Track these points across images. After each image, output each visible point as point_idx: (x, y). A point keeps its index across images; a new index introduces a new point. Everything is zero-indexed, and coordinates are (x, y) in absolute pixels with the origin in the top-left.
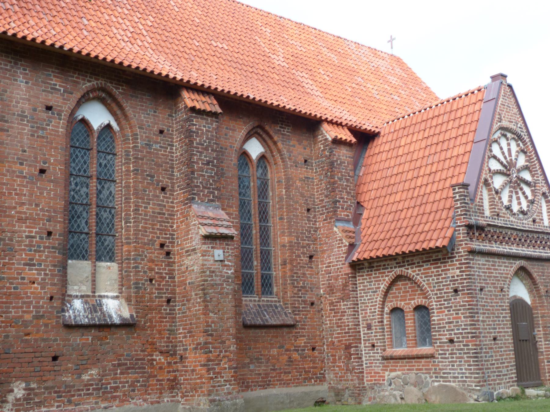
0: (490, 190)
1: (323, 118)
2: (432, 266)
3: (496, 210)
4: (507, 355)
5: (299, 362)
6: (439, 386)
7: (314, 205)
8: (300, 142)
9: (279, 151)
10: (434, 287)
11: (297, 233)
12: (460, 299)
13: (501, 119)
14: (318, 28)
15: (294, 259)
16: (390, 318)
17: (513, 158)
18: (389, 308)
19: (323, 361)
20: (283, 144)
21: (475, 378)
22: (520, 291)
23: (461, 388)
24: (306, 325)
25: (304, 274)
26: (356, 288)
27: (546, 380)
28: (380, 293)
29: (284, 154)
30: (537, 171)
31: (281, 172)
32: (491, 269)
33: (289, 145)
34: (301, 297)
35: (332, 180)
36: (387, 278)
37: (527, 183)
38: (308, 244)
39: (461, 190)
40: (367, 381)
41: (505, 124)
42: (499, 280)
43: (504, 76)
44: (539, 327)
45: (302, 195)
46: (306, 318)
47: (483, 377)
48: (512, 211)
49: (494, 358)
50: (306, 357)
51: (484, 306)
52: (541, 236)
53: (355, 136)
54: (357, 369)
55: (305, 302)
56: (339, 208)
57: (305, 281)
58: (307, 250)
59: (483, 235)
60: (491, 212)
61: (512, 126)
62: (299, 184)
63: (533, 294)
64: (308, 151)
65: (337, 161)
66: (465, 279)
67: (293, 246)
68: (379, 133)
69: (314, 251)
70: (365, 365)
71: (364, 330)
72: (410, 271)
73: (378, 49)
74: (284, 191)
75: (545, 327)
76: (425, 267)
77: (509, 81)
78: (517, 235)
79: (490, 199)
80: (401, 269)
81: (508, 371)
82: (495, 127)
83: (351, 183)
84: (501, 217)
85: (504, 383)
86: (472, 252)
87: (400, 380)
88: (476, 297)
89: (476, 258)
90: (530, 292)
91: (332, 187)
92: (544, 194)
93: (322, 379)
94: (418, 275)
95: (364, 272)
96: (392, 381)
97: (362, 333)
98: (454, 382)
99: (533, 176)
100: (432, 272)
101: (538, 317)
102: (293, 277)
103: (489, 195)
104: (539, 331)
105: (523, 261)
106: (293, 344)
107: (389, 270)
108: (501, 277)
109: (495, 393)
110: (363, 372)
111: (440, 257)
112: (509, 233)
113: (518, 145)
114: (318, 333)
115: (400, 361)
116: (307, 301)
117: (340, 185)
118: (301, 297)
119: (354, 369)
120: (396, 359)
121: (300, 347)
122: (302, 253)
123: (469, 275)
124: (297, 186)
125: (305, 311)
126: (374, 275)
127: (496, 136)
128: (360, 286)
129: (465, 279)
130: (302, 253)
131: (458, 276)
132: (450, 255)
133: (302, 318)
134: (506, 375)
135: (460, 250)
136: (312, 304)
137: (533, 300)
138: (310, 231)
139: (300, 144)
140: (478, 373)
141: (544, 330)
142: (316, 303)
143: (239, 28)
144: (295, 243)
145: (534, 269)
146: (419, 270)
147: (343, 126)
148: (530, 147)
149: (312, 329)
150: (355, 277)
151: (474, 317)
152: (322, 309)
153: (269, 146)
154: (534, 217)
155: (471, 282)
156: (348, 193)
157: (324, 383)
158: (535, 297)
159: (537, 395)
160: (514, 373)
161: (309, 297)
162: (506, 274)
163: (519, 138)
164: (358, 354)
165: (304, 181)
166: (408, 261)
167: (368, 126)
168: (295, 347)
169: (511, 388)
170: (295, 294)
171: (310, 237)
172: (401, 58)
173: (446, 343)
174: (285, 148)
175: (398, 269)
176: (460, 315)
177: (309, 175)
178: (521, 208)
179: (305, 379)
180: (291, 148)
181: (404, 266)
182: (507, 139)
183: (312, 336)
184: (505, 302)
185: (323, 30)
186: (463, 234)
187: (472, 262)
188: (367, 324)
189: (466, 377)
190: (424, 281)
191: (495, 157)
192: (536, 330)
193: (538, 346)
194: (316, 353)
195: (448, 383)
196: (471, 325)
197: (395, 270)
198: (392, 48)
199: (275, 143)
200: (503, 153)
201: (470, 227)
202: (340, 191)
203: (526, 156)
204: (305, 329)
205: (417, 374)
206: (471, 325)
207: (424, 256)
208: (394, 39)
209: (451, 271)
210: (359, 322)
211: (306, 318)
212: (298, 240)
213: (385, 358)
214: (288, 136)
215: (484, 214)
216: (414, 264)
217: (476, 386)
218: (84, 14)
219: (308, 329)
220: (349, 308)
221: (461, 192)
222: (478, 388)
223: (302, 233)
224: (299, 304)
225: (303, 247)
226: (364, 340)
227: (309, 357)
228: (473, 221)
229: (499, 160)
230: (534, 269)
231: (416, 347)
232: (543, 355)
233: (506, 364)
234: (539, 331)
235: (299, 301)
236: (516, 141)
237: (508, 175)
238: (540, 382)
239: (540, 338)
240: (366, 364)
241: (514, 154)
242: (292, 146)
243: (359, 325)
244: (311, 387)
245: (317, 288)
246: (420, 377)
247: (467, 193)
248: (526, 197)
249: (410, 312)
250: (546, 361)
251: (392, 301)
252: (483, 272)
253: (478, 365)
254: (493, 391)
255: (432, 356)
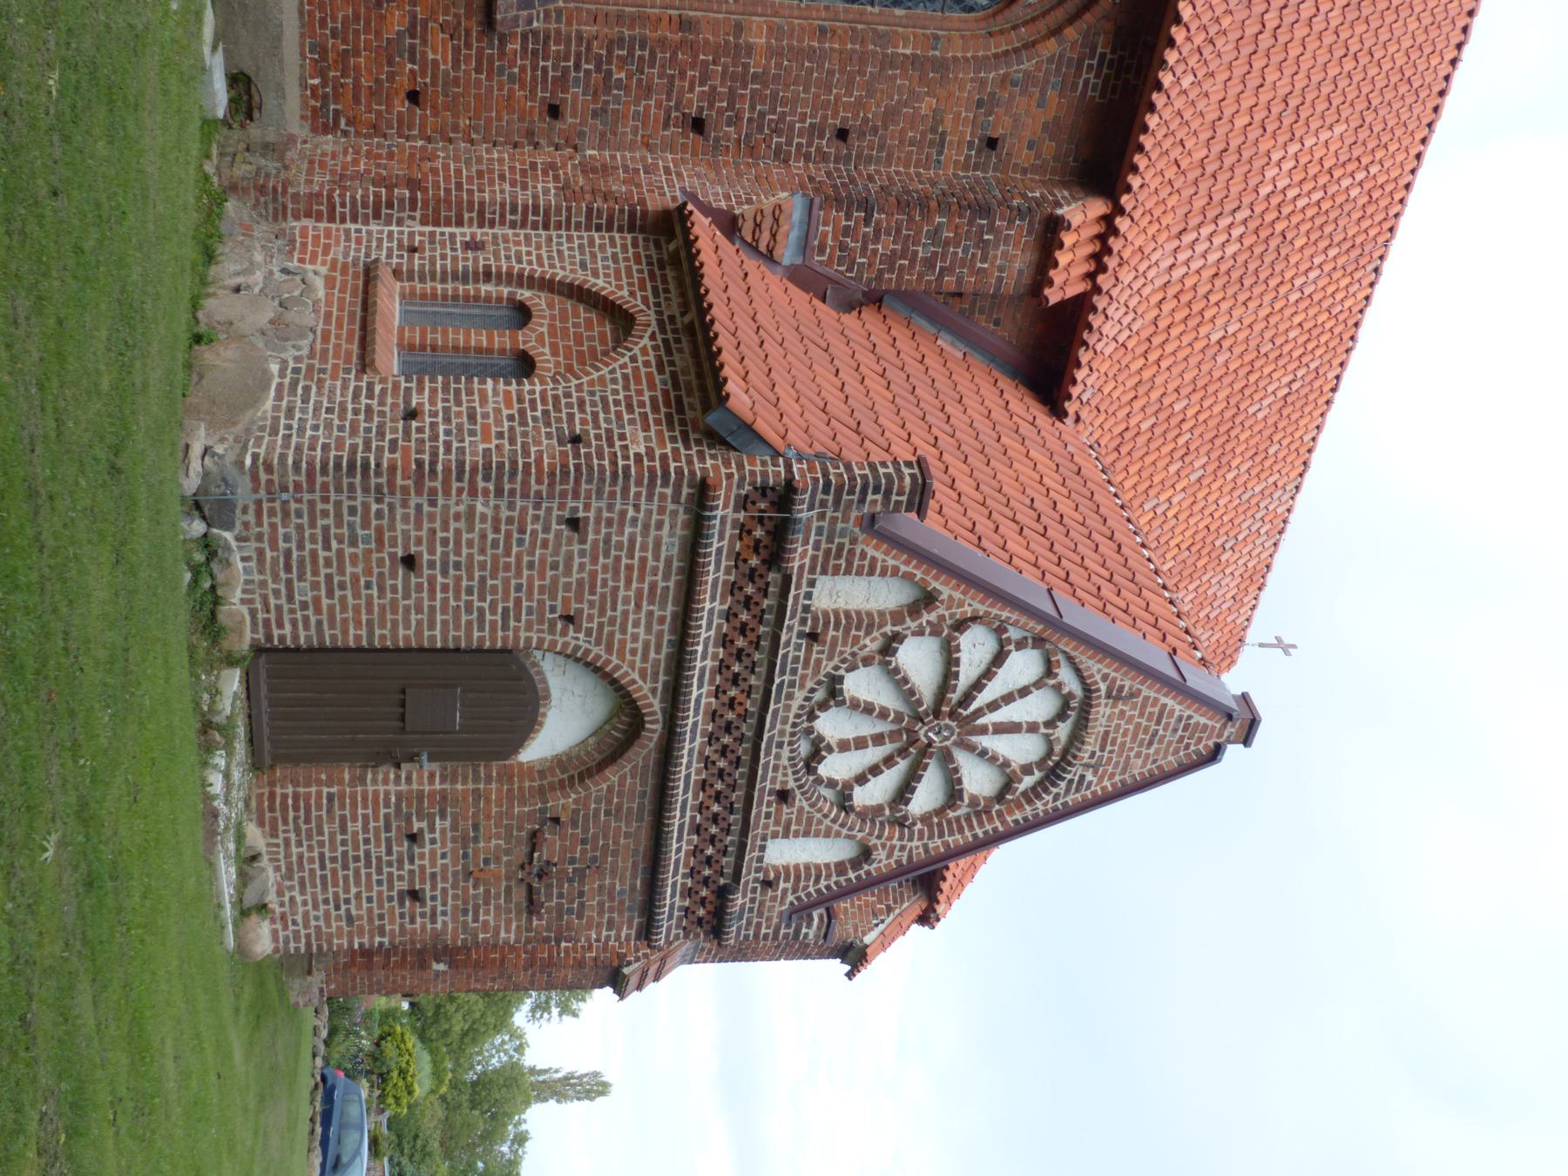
0: (897, 617)
1: (1124, 199)
2: (659, 394)
3: (831, 633)
4: (357, 610)
5: (378, 34)
6: (266, 372)
7: (859, 156)
8: (1051, 128)
9: (1030, 46)
10: (592, 394)
11: (776, 77)
12: (547, 448)
13: (1118, 698)
14: (1338, 396)
15: (696, 57)
16: (499, 299)
17: (985, 741)
18: (531, 299)
19: (376, 129)
20: (1050, 60)
21: (283, 457)
22: (566, 721)
23: (253, 422)
24: (489, 78)
25: (648, 91)
26: (599, 228)
27: (272, 784)
28: (579, 277)
29: (1020, 62)
30: (941, 835)
31: (965, 50)
32: (641, 579)
33: (1046, 81)
34: (577, 67)
35: (933, 204)
36: (625, 293)
37: (904, 792)
38: (739, 117)
39: (908, 480)
40: (304, 230)
41: (1102, 712)
42: (602, 613)
43: (1247, 741)
44: (443, 780)
45: (891, 115)
46: (511, 78)
47: (284, 489)
48: (824, 706)
49: (348, 551)
50: (390, 63)
51: (522, 531)
52: (743, 750)
53: (1062, 304)
54: (342, 196)
55: (562, 82)
56: (848, 217)
57: (627, 88)
58: (720, 111)
59: (754, 561)
60: (826, 614)
61: (1091, 743)
62: (926, 106)
63: (551, 769)
64: (1024, 157)
65: (992, 228)
66: (614, 463)
67: (737, 56)
68: (1059, 413)
69: (717, 140)
70: (353, 227)
71: (463, 235)
72: (646, 341)
73: (1264, 595)
74: (908, 52)
75: (444, 798)
76: (658, 378)
77: (1233, 751)
78: (741, 739)
79: (869, 614)
80: (654, 323)
81: (304, 605)
82: (1095, 668)
83: (921, 276)
84: (809, 650)
85: (263, 584)
86: (703, 492)
87: (296, 293)
88: (551, 496)
89: (682, 517)
90: (560, 762)
91: (914, 204)
92: (866, 854)
93: (321, 122)
94: (633, 359)
95: (646, 248)
96: (298, 278)
97: (457, 230)
98: (276, 408)
99: (925, 819)
100: (640, 393)
101: (476, 780)
102: (642, 48)
103: (881, 614)
104: (432, 776)
105: (658, 727)
106: (433, 15)
107: (651, 300)
108: (612, 621)
109: (228, 535)
110: (331, 219)
111: (689, 415)
112: (757, 656)
113: (1027, 769)
114: (464, 122)
115: (359, 300)
116: (565, 91)
117: (918, 233)
118: (577, 67)
119: (344, 189)
120: (366, 291)
121: (424, 42)
122: (713, 88)
123: (627, 476)
124: (919, 99)
125: (534, 78)
126: (635, 267)
127: (1065, 675)
128: (602, 238)
129: (614, 463)
130: (713, 88)
131: (625, 448)
132: (692, 436)
133: (512, 64)
134: (290, 599)
135: (709, 462)
136: (554, 111)
137: (531, 769)
138: (777, 131)
139: (1045, 127)
140: (297, 464)
141: (432, 794)
142: (558, 125)
143: (1228, 579)
144: (746, 66)
145: (627, 778)
146: (647, 364)
147: (1091, 276)
148: (1018, 816)
149: (477, 97)
150: (631, 229)
151: (487, 478)
152: (536, 145)
153: (1044, 14)
154: (800, 801)
155: (602, 480)
156: (891, 259)
157: (307, 125)
158: (542, 774)
159: (218, 692)
160: (295, 637)
161: (575, 96)
162: (623, 643)
163: (1053, 769)
164: (390, 205)
165: (934, 130)
166: (678, 341)
167: (1088, 383)
168: (425, 22)
169: (244, 610)
170: (589, 48)
171: (760, 129)
172: (1234, 669)
173: (407, 401)
174: (1038, 67)
175: (653, 317)
176: (495, 442)
177: (951, 154)
178: (830, 749)
179: (323, 51)
180: (1036, 91)
181: (663, 330)
182: (1050, 724)
183: (456, 96)
184: (529, 628)
185: (1330, 416)
186: (764, 474)
187: (669, 491)
188: (483, 243)
189: (287, 437)
190: (613, 371)
191: (999, 659)
192: (435, 767)
193: (382, 769)
194: (401, 106)
195: (272, 393)
196: (461, 464)
197: (652, 312)
198: (1261, 645)
199: (1056, 32)
200: (1008, 698)
201: (784, 496)
202: (898, 231)
203: (990, 801)
204: (478, 70)
205: (313, 330)
206: (461, 464)
207: (693, 377)
208: (1287, 653)
209: (641, 435)
210: (492, 224)
211: (511, 78)
212: (755, 76)
213: (369, 275)
214: (1075, 85)
215: (824, 572)
216: (669, 352)
217: (255, 457)
218: (1266, 240)
219: (478, 82)
220: (535, 197)
221: (901, 479)
222: (248, 462)
223: (774, 95)
224: (558, 58)
225: (732, 97)
226: (432, 234)
227: (391, 77)
228: (803, 512)
229: (988, 674)
230: (627, 778)
231: (400, 345)
232: (352, 783)
233: (325, 602)
234: (432, 776)
235: (567, 59)
236: (1041, 763)
237: (937, 713)
238: (268, 760)
239: (409, 779)
240: (358, 231)
241: (1000, 745)
242: (1043, 93)
243: (481, 226)
244: (296, 71)
245: (603, 135)
246: (302, 336)
247: (897, 508)
248: (861, 779)
249: (514, 341)
250: (334, 790)
251: (551, 306)
252: (632, 541)
253: (324, 471)
254: (238, 527)
255: (365, 363)
